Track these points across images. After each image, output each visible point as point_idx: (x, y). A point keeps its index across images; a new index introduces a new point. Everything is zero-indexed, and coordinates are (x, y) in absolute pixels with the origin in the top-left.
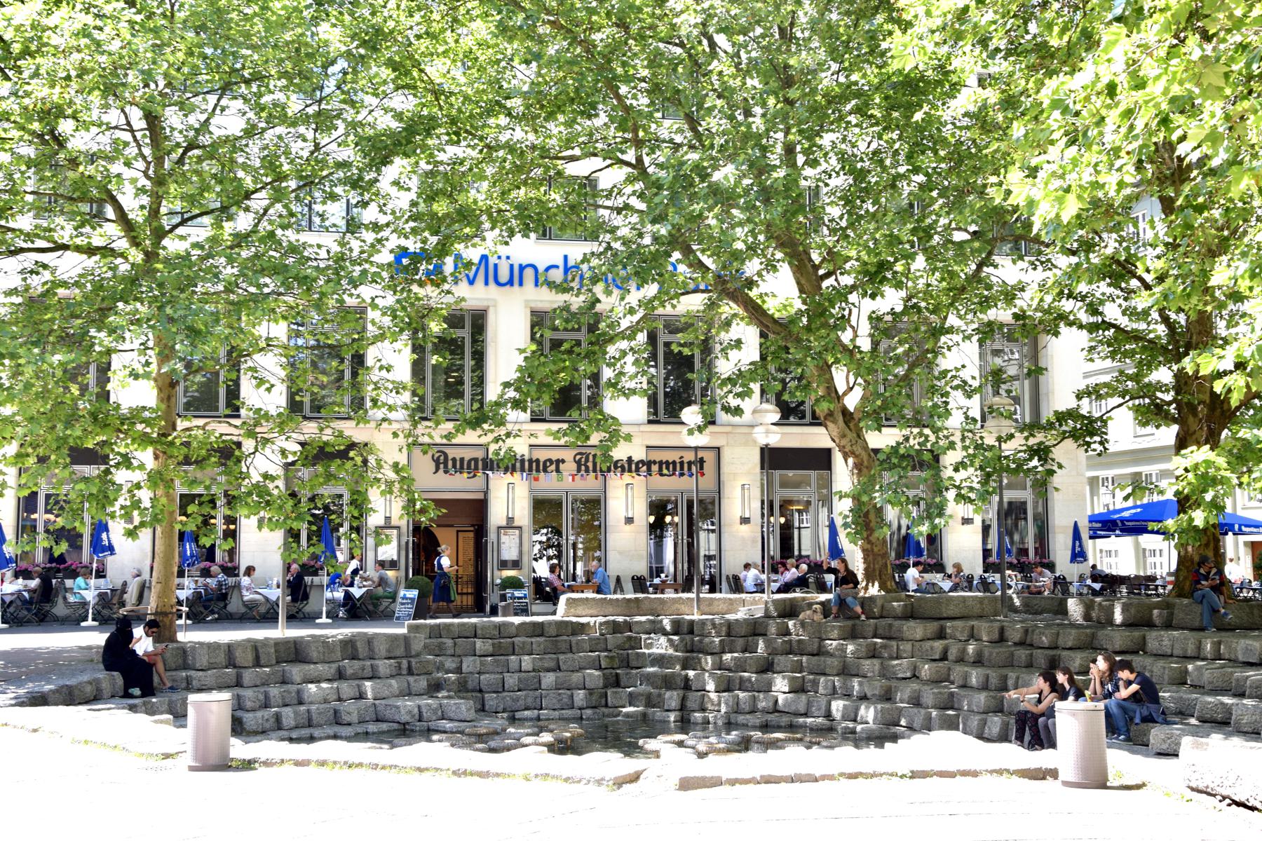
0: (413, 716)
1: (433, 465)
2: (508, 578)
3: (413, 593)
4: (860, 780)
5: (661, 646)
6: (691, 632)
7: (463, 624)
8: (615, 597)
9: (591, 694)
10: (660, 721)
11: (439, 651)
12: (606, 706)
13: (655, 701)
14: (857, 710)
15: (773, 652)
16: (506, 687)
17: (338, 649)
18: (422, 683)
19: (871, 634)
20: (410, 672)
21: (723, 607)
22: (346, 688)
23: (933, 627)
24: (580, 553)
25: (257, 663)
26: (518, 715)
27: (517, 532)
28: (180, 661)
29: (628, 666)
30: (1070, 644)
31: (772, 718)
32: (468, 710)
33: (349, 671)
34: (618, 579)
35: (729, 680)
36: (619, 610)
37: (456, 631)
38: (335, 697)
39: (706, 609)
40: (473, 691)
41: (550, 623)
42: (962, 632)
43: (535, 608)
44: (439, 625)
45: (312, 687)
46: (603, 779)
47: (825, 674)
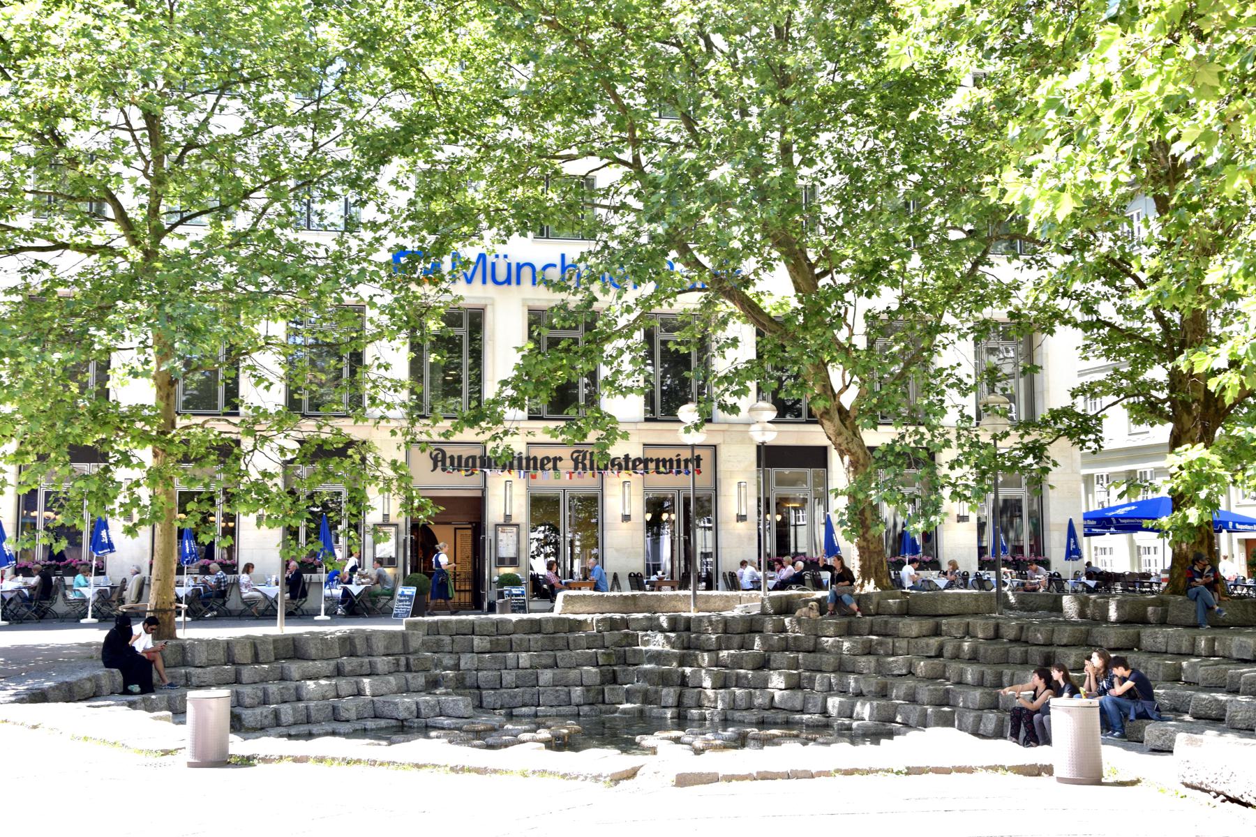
0: (411, 713)
1: (431, 463)
2: (506, 575)
3: (412, 591)
4: (856, 776)
5: (658, 643)
6: (688, 629)
7: (461, 622)
8: (612, 594)
9: (588, 691)
10: (657, 718)
11: (437, 648)
12: (603, 702)
13: (652, 697)
14: (853, 706)
15: (769, 649)
16: (504, 683)
17: (337, 645)
18: (420, 680)
19: (867, 631)
20: (408, 669)
21: (719, 604)
22: (345, 685)
23: (928, 624)
24: (577, 550)
25: (256, 660)
26: (516, 711)
27: (515, 529)
28: (179, 658)
29: (625, 663)
30: (1065, 641)
31: (768, 714)
32: (466, 707)
33: (348, 668)
34: (615, 577)
35: (726, 677)
36: (616, 608)
37: (454, 628)
38: (334, 694)
39: (703, 606)
40: (470, 688)
41: (547, 620)
42: (957, 629)
43: (532, 605)
44: (437, 622)
45: (311, 684)
46: (600, 776)
47: (821, 671)
